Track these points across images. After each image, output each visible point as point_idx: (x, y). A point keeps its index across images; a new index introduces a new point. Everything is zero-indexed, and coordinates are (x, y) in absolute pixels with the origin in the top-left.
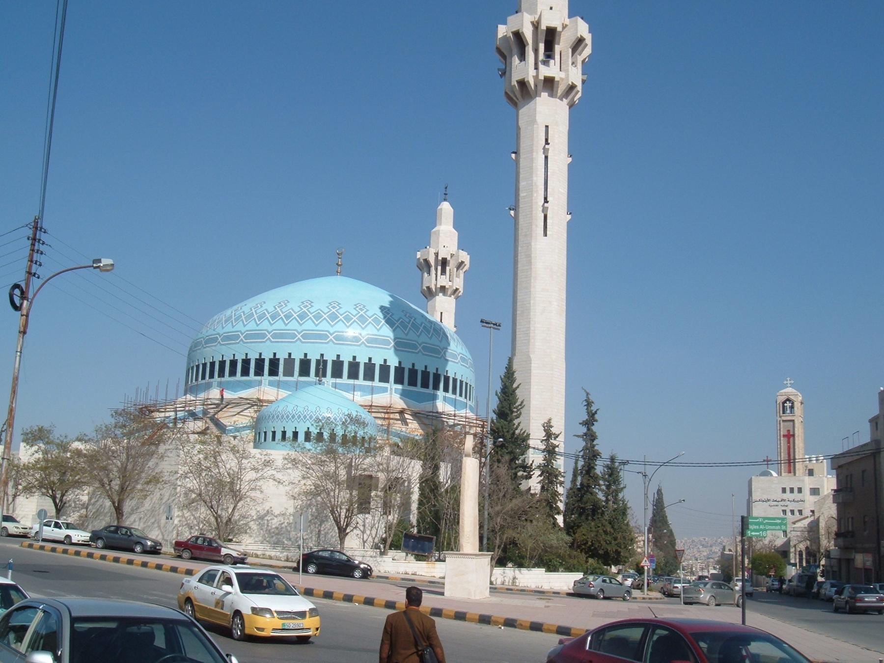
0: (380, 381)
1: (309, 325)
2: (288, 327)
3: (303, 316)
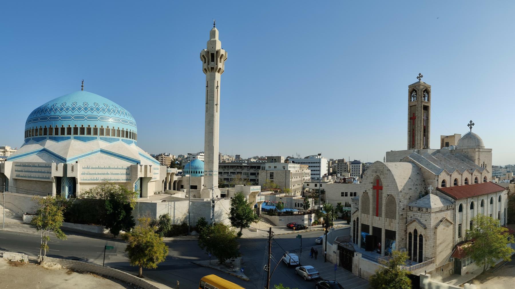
0: (61, 134)
1: (76, 113)
2: (80, 114)
3: (73, 109)
